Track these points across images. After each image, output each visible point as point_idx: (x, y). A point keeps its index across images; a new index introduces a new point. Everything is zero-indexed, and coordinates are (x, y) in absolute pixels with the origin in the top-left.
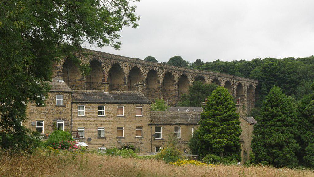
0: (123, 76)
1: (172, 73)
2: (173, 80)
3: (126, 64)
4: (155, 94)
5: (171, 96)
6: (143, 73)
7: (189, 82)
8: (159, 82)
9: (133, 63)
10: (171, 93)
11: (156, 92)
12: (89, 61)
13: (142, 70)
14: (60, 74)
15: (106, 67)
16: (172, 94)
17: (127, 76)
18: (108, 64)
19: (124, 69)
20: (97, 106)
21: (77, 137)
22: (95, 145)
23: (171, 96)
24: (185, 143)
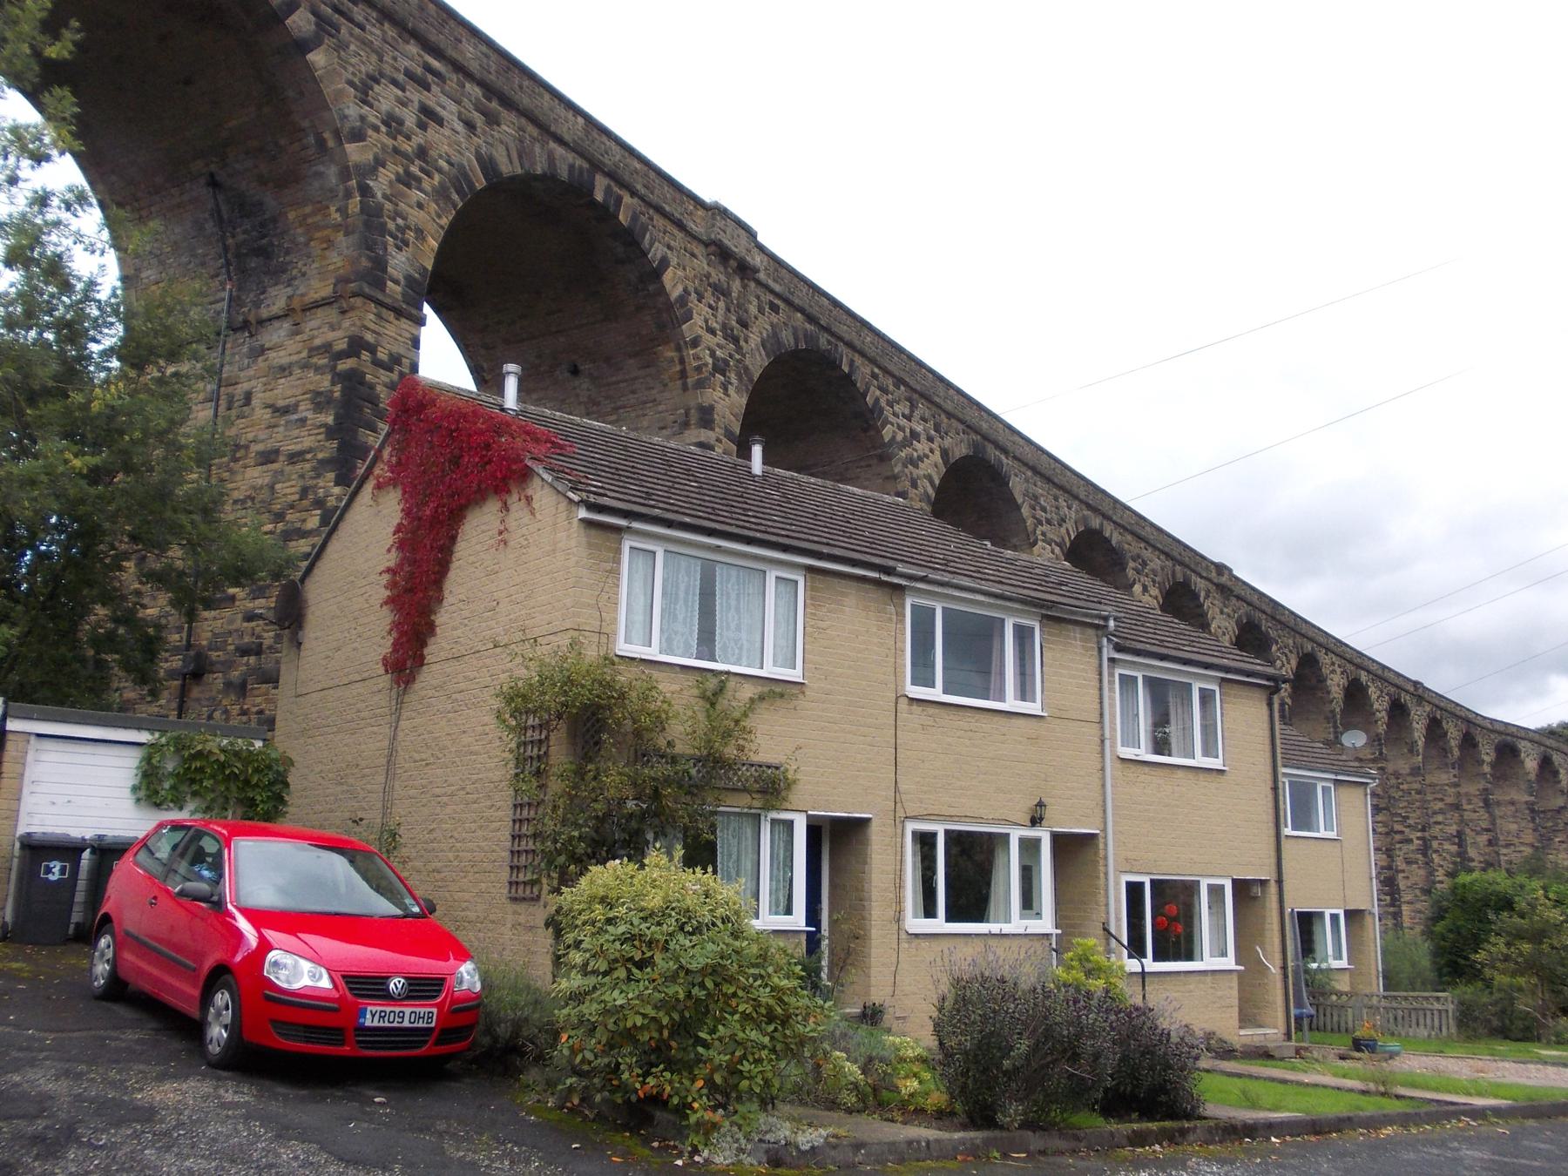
0: (1327, 708)
1: (1444, 723)
2: (1444, 749)
3: (1333, 664)
4: (1400, 793)
5: (1440, 805)
6: (1376, 706)
7: (1483, 761)
8: (1412, 750)
9: (1350, 662)
10: (1440, 796)
11: (1405, 787)
12: (1237, 623)
13: (1374, 697)
14: (1445, 970)
15: (1284, 659)
16: (1442, 800)
17: (1338, 710)
18: (1286, 651)
19: (1329, 682)
20: (1366, 895)
21: (720, 690)
22: (358, 688)
23: (1440, 805)
24: (922, 1060)
